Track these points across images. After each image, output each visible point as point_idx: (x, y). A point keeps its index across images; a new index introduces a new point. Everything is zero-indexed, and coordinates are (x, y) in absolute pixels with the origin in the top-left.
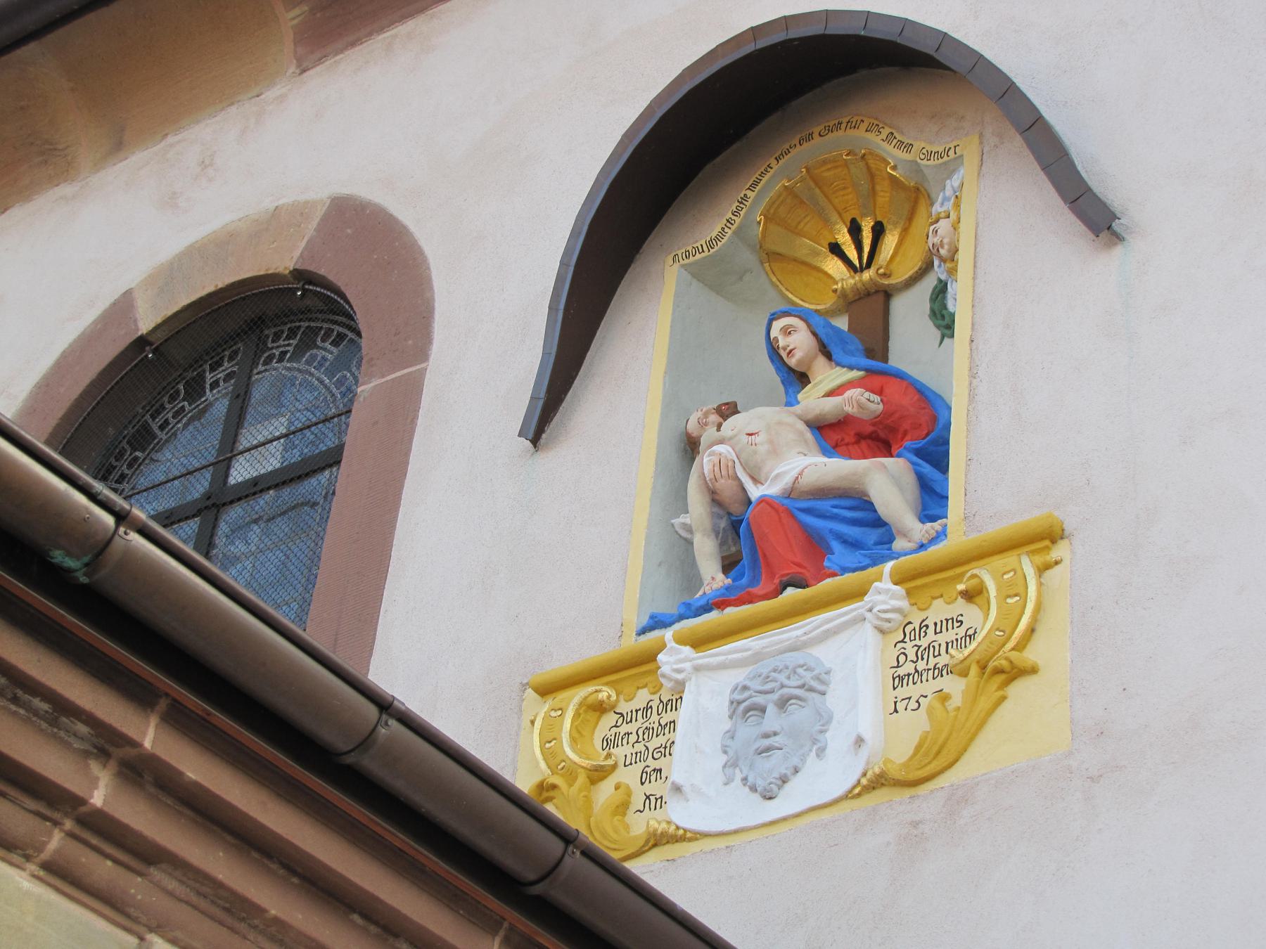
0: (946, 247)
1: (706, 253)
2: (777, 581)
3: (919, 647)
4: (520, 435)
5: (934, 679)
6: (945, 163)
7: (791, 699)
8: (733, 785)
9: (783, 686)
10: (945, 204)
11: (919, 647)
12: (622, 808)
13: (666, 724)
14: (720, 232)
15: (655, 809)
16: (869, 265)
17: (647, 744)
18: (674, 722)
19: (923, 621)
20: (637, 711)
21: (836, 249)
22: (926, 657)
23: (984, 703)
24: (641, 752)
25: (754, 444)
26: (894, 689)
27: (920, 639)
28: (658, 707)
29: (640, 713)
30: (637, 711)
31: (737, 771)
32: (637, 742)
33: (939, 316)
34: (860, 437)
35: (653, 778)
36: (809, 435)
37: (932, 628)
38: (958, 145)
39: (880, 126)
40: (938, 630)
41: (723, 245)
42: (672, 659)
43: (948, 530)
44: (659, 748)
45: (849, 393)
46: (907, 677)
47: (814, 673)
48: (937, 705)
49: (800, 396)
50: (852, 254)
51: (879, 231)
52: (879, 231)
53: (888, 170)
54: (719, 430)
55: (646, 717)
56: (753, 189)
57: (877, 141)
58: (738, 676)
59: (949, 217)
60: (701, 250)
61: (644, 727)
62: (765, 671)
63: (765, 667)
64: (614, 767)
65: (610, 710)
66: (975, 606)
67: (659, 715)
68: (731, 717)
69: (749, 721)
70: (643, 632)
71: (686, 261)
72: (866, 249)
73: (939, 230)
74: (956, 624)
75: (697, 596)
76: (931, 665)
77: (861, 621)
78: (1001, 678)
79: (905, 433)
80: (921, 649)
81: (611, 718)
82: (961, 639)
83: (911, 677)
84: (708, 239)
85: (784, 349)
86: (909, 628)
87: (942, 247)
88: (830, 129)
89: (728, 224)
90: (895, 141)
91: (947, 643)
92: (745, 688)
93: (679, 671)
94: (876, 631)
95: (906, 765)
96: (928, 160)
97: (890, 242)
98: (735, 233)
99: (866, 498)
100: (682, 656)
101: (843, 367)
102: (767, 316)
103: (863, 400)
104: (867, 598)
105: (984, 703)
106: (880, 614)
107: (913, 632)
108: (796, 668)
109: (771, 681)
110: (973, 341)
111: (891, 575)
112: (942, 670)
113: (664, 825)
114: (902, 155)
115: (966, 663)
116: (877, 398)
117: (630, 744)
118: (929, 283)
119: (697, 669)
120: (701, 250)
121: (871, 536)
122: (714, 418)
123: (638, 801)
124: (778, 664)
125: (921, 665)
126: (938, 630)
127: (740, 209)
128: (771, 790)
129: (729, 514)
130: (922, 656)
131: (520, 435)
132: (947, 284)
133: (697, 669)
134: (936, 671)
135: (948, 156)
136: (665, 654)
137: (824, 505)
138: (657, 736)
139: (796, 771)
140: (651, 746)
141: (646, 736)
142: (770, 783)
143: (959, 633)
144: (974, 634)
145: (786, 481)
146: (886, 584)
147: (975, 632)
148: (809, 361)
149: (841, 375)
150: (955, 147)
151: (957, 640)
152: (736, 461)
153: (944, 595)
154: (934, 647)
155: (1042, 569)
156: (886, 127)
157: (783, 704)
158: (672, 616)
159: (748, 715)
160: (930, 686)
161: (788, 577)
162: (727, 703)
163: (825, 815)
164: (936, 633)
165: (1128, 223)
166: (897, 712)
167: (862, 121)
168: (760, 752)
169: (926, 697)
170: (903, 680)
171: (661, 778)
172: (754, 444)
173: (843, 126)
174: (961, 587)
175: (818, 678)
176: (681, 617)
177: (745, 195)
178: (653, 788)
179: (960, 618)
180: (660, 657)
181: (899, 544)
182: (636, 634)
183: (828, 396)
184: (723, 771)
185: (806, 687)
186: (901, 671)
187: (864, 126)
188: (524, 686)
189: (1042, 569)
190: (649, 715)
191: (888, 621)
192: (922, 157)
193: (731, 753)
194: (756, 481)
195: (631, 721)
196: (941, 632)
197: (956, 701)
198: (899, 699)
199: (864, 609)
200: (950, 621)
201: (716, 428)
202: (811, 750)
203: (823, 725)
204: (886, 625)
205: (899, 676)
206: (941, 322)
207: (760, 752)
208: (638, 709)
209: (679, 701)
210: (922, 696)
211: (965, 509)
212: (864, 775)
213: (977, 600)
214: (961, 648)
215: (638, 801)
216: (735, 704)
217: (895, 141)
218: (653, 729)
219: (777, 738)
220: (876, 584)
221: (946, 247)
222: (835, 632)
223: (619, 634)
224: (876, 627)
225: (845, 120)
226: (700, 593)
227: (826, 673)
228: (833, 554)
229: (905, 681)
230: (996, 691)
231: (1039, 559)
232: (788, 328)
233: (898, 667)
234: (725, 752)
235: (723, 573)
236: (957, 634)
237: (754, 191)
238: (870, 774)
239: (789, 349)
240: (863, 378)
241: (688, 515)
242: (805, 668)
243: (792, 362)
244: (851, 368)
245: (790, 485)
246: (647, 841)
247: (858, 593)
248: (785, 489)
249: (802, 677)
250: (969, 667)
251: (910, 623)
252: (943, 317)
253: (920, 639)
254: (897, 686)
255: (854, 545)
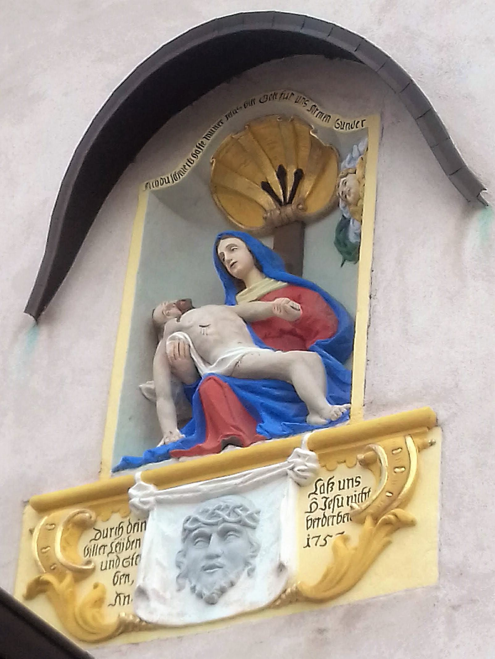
0: (352, 195)
1: (171, 184)
2: (220, 440)
3: (327, 498)
4: (25, 312)
5: (338, 523)
6: (354, 132)
7: (228, 532)
8: (184, 591)
9: (224, 521)
10: (352, 162)
11: (327, 498)
12: (99, 602)
13: (134, 541)
14: (182, 169)
15: (124, 604)
16: (290, 201)
17: (118, 555)
18: (139, 540)
19: (330, 479)
20: (111, 529)
21: (266, 187)
22: (332, 506)
23: (376, 545)
24: (113, 561)
25: (205, 334)
26: (308, 528)
27: (328, 493)
28: (128, 527)
29: (114, 531)
30: (111, 529)
31: (187, 581)
32: (111, 552)
33: (342, 244)
34: (283, 332)
35: (123, 581)
36: (246, 329)
37: (337, 484)
38: (364, 120)
39: (306, 100)
40: (342, 487)
41: (184, 179)
42: (140, 493)
43: (351, 413)
44: (127, 559)
45: (277, 301)
46: (317, 520)
47: (248, 512)
48: (340, 544)
49: (238, 297)
50: (279, 191)
51: (299, 176)
52: (299, 176)
53: (311, 133)
54: (178, 320)
55: (118, 534)
56: (209, 138)
57: (303, 109)
58: (191, 511)
59: (355, 173)
60: (167, 181)
61: (116, 543)
62: (211, 508)
63: (211, 505)
64: (93, 570)
65: (91, 527)
66: (370, 472)
67: (128, 533)
68: (184, 540)
69: (197, 544)
70: (117, 470)
71: (156, 189)
72: (289, 189)
73: (347, 183)
74: (355, 484)
75: (159, 446)
76: (336, 513)
77: (284, 476)
78: (388, 528)
79: (317, 333)
80: (329, 500)
81: (92, 534)
82: (359, 495)
83: (320, 521)
84: (173, 173)
85: (229, 261)
86: (319, 484)
87: (349, 195)
88: (268, 98)
89: (188, 163)
90: (317, 112)
91: (348, 497)
92: (196, 520)
93: (144, 503)
94: (296, 484)
95: (316, 587)
96: (341, 129)
97: (306, 186)
98: (194, 170)
99: (288, 382)
100: (149, 492)
101: (271, 278)
102: (216, 237)
103: (288, 306)
104: (290, 459)
105: (376, 545)
106: (300, 473)
107: (322, 487)
108: (235, 508)
109: (215, 516)
110: (373, 271)
111: (308, 443)
112: (344, 517)
113: (131, 618)
114: (324, 124)
115: (364, 514)
116: (297, 306)
117: (106, 554)
118: (334, 220)
119: (159, 502)
120: (167, 181)
121: (291, 409)
122: (175, 310)
123: (110, 597)
124: (222, 504)
125: (328, 512)
126: (342, 487)
127: (198, 152)
128: (213, 598)
129: (183, 383)
130: (329, 505)
131: (25, 312)
132: (349, 221)
133: (159, 502)
134: (340, 518)
135: (357, 127)
136: (134, 489)
137: (258, 384)
138: (126, 549)
139: (232, 584)
140: (123, 556)
141: (118, 548)
142: (213, 593)
143: (357, 490)
144: (369, 492)
145: (229, 364)
146: (304, 451)
147: (369, 491)
148: (246, 271)
149: (270, 285)
150: (362, 122)
151: (355, 495)
152: (191, 345)
153: (347, 462)
154: (338, 499)
155: (421, 448)
156: (310, 101)
157: (224, 534)
158: (137, 459)
159: (197, 540)
160: (335, 528)
161: (229, 438)
162: (181, 529)
163: (254, 620)
164: (340, 489)
165: (491, 192)
166: (309, 546)
167: (293, 94)
168: (205, 569)
169: (331, 536)
170: (314, 522)
171: (128, 581)
172: (205, 334)
173: (278, 96)
174: (361, 456)
175: (251, 517)
176: (147, 462)
177: (202, 142)
178: (125, 588)
179: (358, 479)
180: (131, 491)
181: (313, 419)
182: (112, 472)
183: (259, 300)
184: (177, 581)
185: (241, 523)
186: (313, 516)
187: (293, 99)
188: (26, 503)
189: (421, 448)
190: (120, 533)
191: (305, 478)
192: (337, 126)
193: (183, 567)
194: (207, 362)
195: (106, 536)
196: (344, 488)
197: (355, 541)
198: (311, 537)
199: (287, 468)
200: (351, 481)
201: (176, 319)
202: (244, 570)
203: (253, 552)
204: (302, 481)
205: (311, 519)
206: (344, 249)
207: (205, 569)
208: (112, 527)
209: (144, 524)
210: (328, 535)
211: (364, 398)
212: (284, 591)
213: (373, 467)
214: (359, 502)
215: (110, 597)
216: (187, 531)
217: (317, 112)
218: (123, 544)
219: (219, 560)
220: (297, 450)
221: (352, 195)
222: (264, 483)
223: (99, 470)
224: (295, 482)
225: (280, 92)
226: (161, 443)
227: (256, 513)
228: (263, 422)
229: (316, 524)
230: (384, 537)
231: (419, 441)
232: (232, 247)
233: (311, 512)
234: (179, 566)
235: (179, 428)
236: (355, 491)
237: (209, 140)
238: (289, 590)
239: (232, 262)
240: (284, 288)
241: (153, 381)
242: (241, 508)
243: (234, 272)
244: (277, 279)
245: (232, 367)
246: (118, 629)
247: (284, 454)
248: (229, 370)
249: (239, 515)
250: (365, 519)
251: (320, 480)
252: (346, 245)
253: (328, 493)
254: (310, 527)
255: (278, 416)
